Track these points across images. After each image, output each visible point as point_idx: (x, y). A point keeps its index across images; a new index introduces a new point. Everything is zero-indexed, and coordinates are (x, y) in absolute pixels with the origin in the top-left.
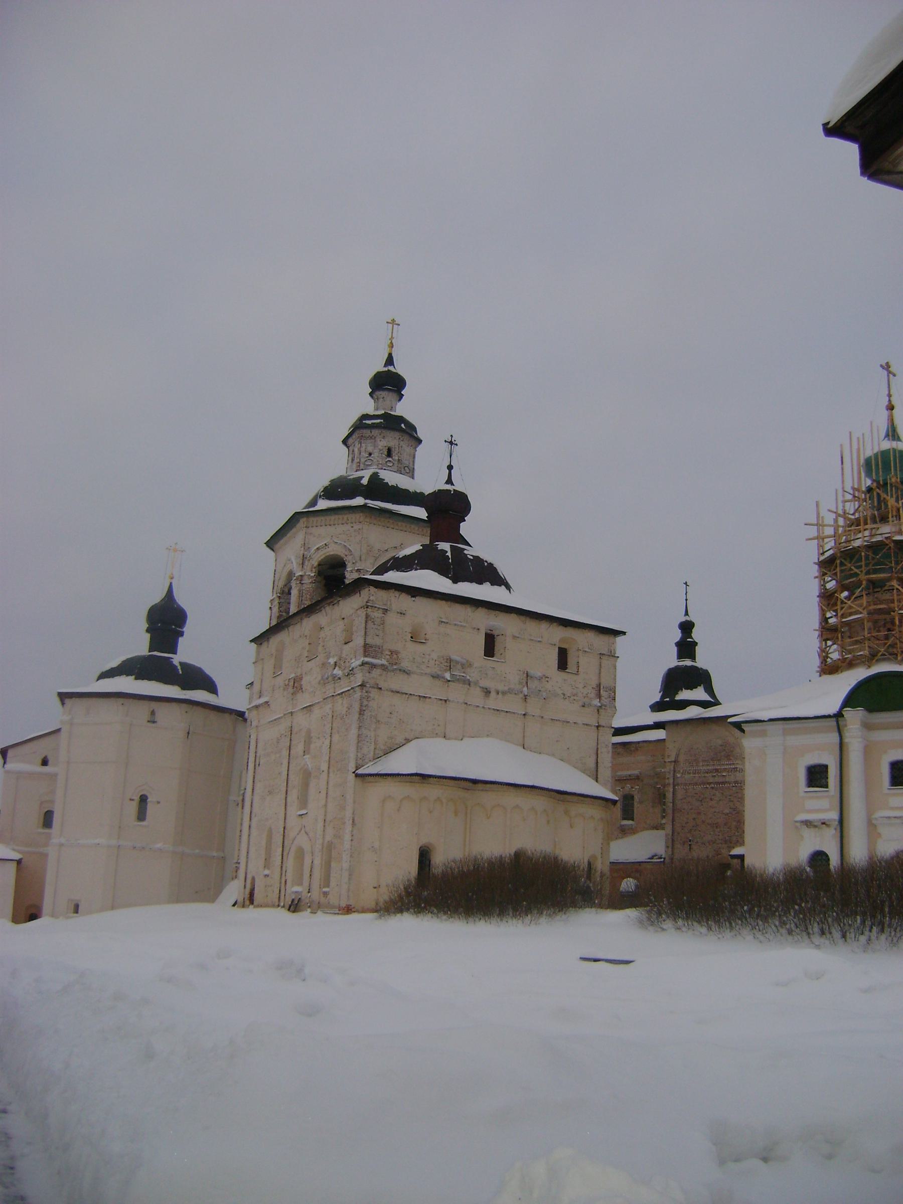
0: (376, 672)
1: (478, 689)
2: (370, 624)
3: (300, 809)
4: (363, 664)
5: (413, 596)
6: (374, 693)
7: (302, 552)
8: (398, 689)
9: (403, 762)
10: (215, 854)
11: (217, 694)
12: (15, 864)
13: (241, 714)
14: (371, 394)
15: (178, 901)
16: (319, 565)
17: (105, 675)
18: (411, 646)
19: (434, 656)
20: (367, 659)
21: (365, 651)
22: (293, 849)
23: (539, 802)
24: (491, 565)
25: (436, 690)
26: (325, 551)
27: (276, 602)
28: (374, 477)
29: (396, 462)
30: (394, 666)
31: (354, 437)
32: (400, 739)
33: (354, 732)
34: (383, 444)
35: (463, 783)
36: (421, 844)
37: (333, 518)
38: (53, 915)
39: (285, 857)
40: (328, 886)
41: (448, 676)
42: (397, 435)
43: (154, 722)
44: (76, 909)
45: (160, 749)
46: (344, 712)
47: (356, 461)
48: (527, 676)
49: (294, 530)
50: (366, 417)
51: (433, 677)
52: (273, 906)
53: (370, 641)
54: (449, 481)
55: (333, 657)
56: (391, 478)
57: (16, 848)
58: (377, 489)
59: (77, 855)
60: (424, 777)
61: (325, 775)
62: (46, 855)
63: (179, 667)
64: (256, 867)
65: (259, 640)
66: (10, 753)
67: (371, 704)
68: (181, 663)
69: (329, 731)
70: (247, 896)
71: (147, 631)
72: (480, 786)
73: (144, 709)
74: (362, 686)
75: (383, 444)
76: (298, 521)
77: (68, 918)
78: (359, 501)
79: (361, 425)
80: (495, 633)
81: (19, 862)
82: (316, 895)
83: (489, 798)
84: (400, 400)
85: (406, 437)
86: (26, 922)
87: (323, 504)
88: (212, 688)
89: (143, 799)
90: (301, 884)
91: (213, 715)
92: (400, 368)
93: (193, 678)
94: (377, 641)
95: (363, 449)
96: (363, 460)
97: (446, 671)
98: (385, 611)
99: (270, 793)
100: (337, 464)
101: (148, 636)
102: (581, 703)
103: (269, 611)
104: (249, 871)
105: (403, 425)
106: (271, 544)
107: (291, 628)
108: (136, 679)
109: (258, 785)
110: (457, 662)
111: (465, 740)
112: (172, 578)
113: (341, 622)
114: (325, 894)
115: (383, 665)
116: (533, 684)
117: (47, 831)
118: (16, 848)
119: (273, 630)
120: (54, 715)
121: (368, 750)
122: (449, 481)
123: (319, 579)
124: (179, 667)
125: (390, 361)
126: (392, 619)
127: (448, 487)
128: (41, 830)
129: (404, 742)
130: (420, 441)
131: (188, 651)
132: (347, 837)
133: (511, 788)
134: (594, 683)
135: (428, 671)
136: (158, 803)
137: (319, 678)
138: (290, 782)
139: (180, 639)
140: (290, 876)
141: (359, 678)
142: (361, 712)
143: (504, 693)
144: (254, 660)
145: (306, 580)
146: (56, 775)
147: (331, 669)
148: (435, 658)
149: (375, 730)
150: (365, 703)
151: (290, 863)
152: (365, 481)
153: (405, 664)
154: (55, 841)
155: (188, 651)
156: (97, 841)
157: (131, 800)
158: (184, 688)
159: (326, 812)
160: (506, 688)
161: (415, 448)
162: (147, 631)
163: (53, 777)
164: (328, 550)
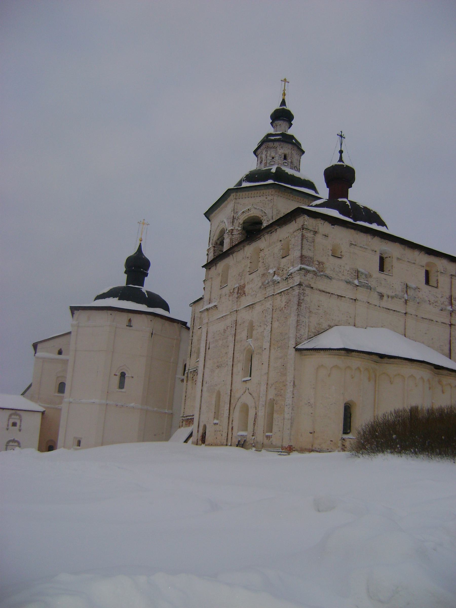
0: (310, 276)
1: (376, 293)
2: (305, 241)
3: (245, 377)
4: (301, 269)
5: (332, 225)
6: (308, 291)
7: (232, 215)
8: (324, 290)
9: (332, 339)
10: (167, 411)
11: (169, 311)
12: (40, 415)
13: (184, 324)
14: (272, 124)
15: (143, 441)
16: (244, 223)
18: (332, 259)
19: (348, 268)
20: (303, 266)
21: (302, 260)
22: (239, 404)
23: (425, 373)
24: (375, 213)
25: (349, 293)
26: (247, 214)
27: (212, 250)
28: (278, 169)
29: (289, 164)
30: (320, 272)
31: (262, 148)
32: (325, 326)
33: (292, 320)
34: (281, 151)
35: (374, 357)
36: (345, 401)
37: (253, 193)
39: (231, 411)
40: (271, 432)
41: (356, 282)
42: (290, 146)
44: (79, 443)
45: (135, 340)
47: (263, 162)
48: (407, 286)
49: (226, 202)
50: (269, 135)
51: (347, 282)
52: (222, 445)
53: (305, 253)
54: (341, 160)
55: (272, 268)
56: (290, 171)
57: (41, 404)
58: (280, 176)
59: (80, 409)
60: (348, 351)
61: (267, 352)
62: (60, 410)
63: (146, 294)
64: (207, 418)
65: (208, 266)
66: (39, 347)
67: (305, 298)
69: (270, 320)
70: (200, 438)
71: (125, 273)
72: (386, 360)
73: (125, 317)
74: (300, 285)
75: (281, 151)
76: (229, 196)
78: (270, 182)
79: (267, 140)
80: (384, 256)
81: (43, 413)
82: (260, 437)
83: (392, 369)
84: (289, 128)
85: (295, 148)
86: (46, 451)
87: (245, 184)
88: (166, 307)
89: (123, 375)
90: (246, 430)
91: (167, 323)
92: (289, 107)
93: (155, 301)
94: (310, 254)
95: (268, 155)
96: (268, 161)
97: (355, 279)
98: (315, 233)
99: (218, 367)
100: (252, 164)
101: (126, 275)
102: (440, 308)
103: (206, 257)
104: (201, 420)
105: (294, 141)
106: (208, 214)
107: (234, 255)
110: (362, 273)
111: (368, 328)
113: (279, 244)
114: (268, 437)
115: (314, 271)
116: (411, 292)
118: (41, 404)
120: (66, 323)
121: (304, 332)
122: (341, 160)
123: (244, 232)
124: (146, 294)
125: (283, 103)
126: (319, 238)
127: (341, 163)
128: (57, 394)
129: (328, 327)
130: (303, 152)
131: (150, 285)
132: (289, 395)
133: (408, 363)
134: (447, 294)
135: (343, 278)
136: (132, 377)
137: (260, 284)
140: (236, 424)
141: (297, 280)
142: (299, 304)
143: (392, 297)
145: (235, 232)
147: (271, 277)
148: (348, 269)
149: (309, 318)
150: (302, 298)
151: (236, 415)
152: (274, 170)
153: (328, 272)
154: (65, 400)
155: (150, 285)
157: (115, 375)
158: (149, 306)
159: (268, 378)
160: (393, 294)
161: (301, 156)
162: (125, 273)
163: (66, 362)
164: (250, 213)
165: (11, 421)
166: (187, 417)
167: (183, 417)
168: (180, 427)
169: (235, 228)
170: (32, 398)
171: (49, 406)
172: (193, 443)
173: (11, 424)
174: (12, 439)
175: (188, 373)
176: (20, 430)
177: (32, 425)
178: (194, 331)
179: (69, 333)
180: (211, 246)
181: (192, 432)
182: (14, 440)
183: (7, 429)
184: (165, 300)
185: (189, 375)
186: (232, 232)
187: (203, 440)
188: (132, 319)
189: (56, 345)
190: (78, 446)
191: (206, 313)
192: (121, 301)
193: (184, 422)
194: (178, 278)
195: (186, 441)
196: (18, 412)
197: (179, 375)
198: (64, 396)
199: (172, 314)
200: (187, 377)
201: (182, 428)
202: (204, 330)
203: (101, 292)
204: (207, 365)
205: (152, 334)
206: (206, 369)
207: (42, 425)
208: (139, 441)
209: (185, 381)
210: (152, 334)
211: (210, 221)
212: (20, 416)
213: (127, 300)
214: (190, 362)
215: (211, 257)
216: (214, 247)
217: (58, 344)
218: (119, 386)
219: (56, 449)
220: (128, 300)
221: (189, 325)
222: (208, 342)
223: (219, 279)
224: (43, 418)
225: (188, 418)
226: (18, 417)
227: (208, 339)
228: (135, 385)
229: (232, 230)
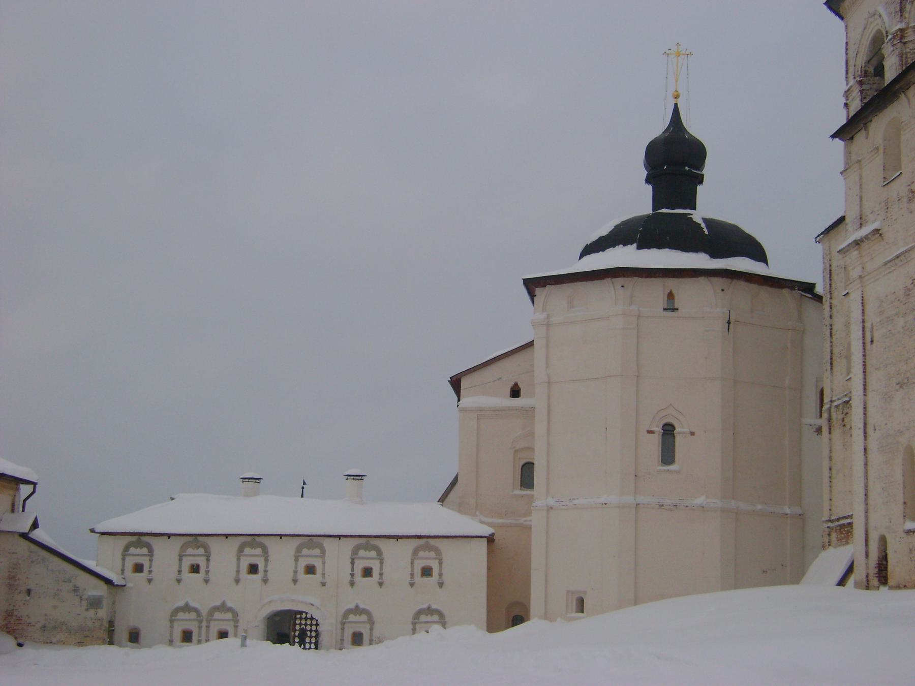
10: (788, 511)
12: (484, 542)
13: (808, 288)
15: (736, 586)
17: (589, 250)
27: (856, 93)
38: (547, 616)
43: (674, 310)
44: (581, 606)
45: (686, 343)
57: (484, 519)
63: (703, 225)
64: (886, 516)
65: (845, 133)
66: (464, 383)
68: (705, 220)
70: (873, 571)
71: (648, 181)
73: (656, 289)
77: (570, 619)
81: (490, 539)
88: (757, 252)
89: (668, 430)
91: (765, 293)
93: (727, 240)
99: (901, 385)
101: (650, 188)
108: (639, 248)
112: (676, 97)
117: (528, 492)
118: (484, 519)
119: (846, 170)
120: (519, 320)
124: (703, 225)
131: (711, 204)
136: (692, 434)
144: (842, 169)
146: (533, 409)
154: (538, 503)
155: (711, 204)
156: (603, 500)
158: (714, 255)
162: (648, 181)
165: (419, 564)
166: (838, 520)
167: (830, 521)
168: (824, 547)
169: (908, 24)
170: (462, 508)
171: (500, 521)
172: (857, 585)
173: (418, 572)
174: (425, 606)
175: (829, 409)
176: (441, 585)
177: (468, 568)
178: (834, 302)
179: (531, 344)
180: (852, 82)
181: (853, 563)
182: (429, 608)
183: (412, 585)
184: (753, 235)
185: (834, 415)
186: (902, 37)
187: (882, 575)
188: (674, 292)
189: (497, 377)
190: (577, 612)
191: (854, 254)
192: (645, 252)
193: (834, 535)
194: (779, 179)
195: (842, 582)
196: (432, 542)
197: (810, 418)
198: (533, 496)
199: (775, 269)
200: (829, 419)
201: (831, 550)
202: (855, 296)
203: (594, 237)
204: (873, 383)
205: (729, 323)
206: (870, 394)
207: (489, 568)
208: (724, 588)
209: (825, 430)
210: (729, 323)
211: (842, 18)
212: (437, 551)
213: (649, 248)
214: (831, 381)
215: (856, 106)
216: (861, 83)
217: (509, 372)
218: (663, 456)
219: (528, 619)
220: (660, 246)
221: (819, 290)
222: (868, 325)
223: (879, 160)
224: (490, 552)
225: (842, 522)
226: (432, 554)
227: (866, 318)
228: (699, 452)
229: (901, 30)
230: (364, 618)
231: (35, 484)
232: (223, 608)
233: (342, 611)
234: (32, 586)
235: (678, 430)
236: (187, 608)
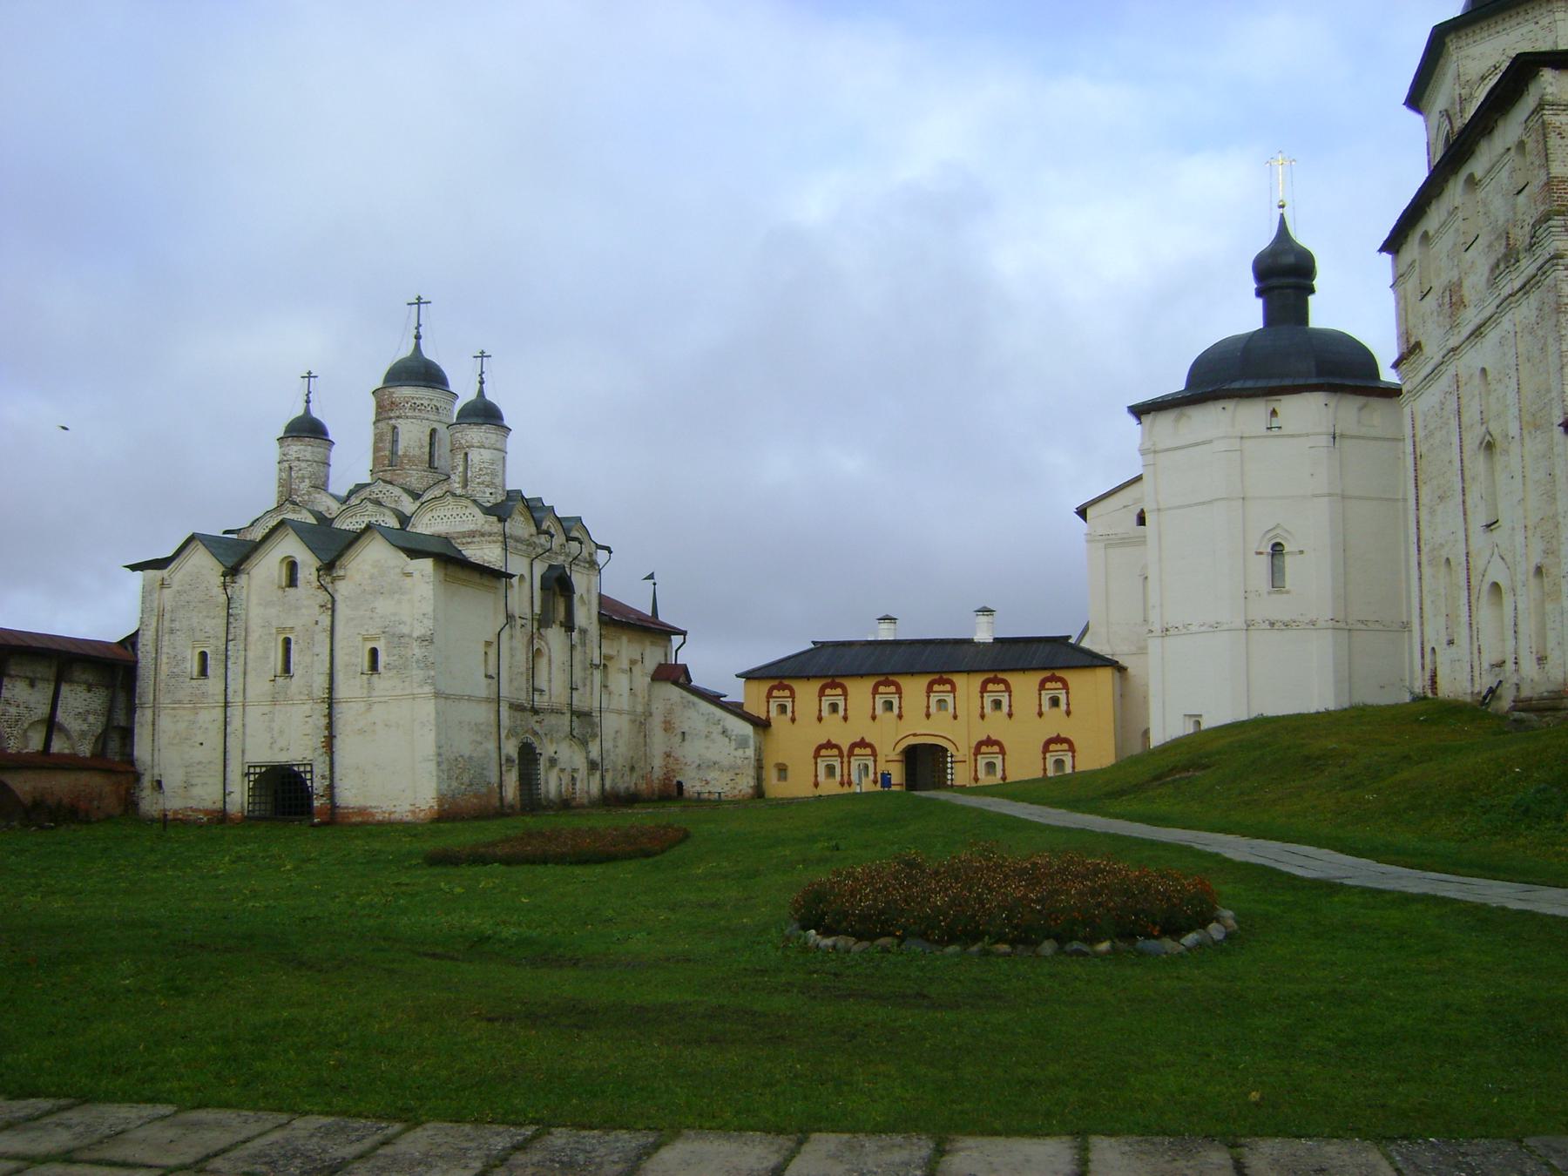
46: (1533, 319)
66: (1089, 512)
89: (1277, 549)
101: (1260, 302)
109: (1424, 490)
112: (1282, 207)
138: (1466, 472)
139: (1311, 298)
155: (1323, 313)
162: (1312, 291)
194: (1355, 302)
204: (1424, 499)
226: (1059, 685)
230: (996, 749)
231: (684, 633)
232: (862, 744)
233: (974, 744)
234: (685, 729)
235: (1287, 549)
236: (829, 745)
